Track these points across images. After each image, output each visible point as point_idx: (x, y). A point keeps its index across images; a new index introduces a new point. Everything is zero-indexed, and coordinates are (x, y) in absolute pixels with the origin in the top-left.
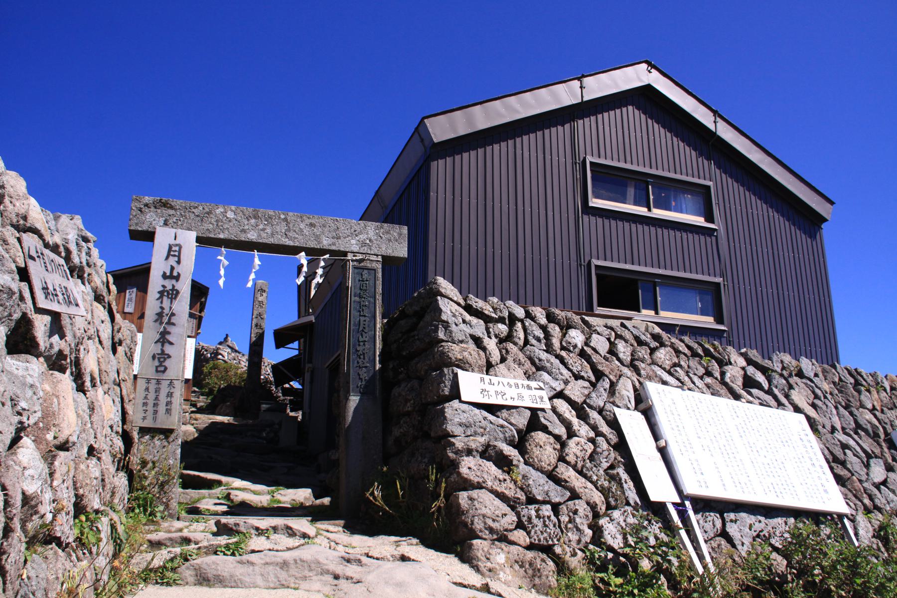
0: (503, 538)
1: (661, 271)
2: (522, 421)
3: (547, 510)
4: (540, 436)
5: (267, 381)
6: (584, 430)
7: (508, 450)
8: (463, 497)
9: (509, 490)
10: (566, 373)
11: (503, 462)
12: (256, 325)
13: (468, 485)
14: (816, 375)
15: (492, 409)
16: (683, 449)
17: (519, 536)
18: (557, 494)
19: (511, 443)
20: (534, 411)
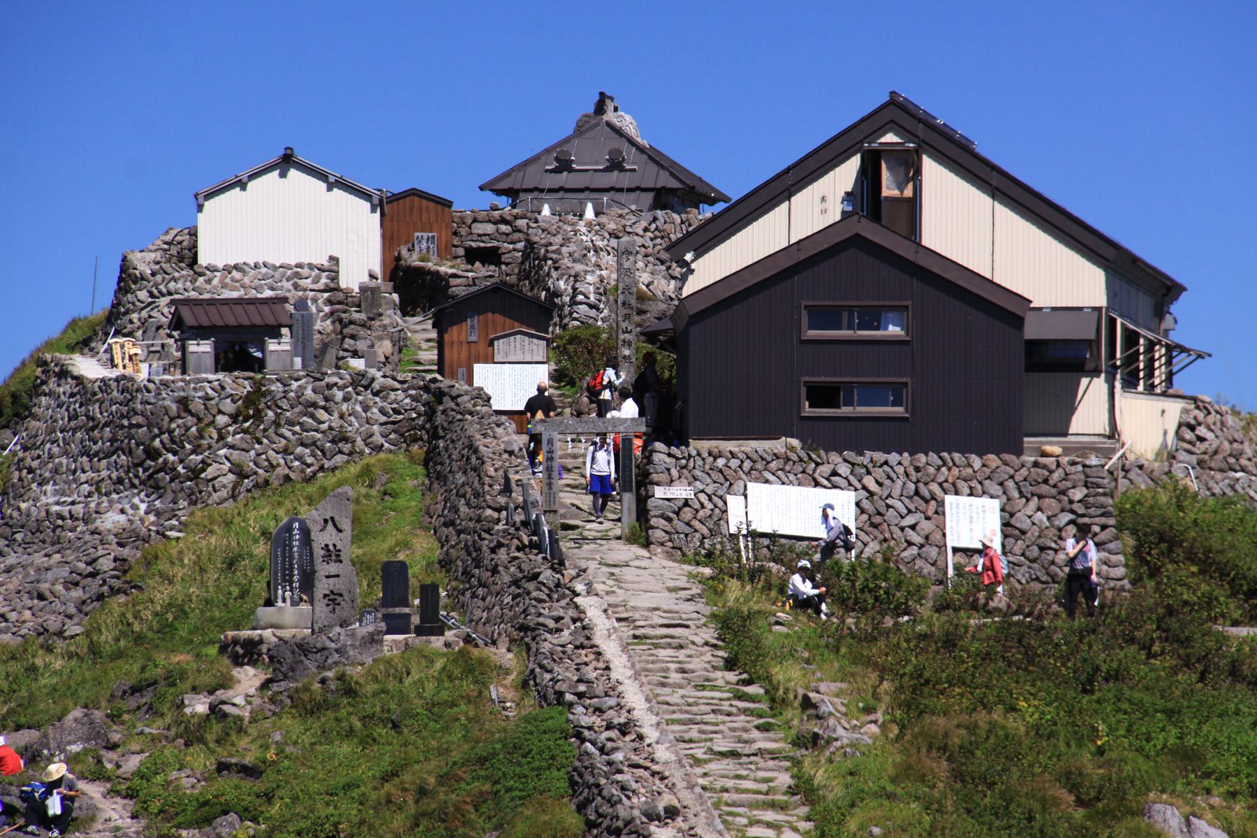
0: (662, 544)
1: (856, 380)
2: (680, 504)
3: (682, 536)
4: (687, 509)
5: (886, 328)
6: (710, 506)
7: (672, 515)
8: (650, 532)
9: (669, 528)
10: (709, 480)
11: (669, 520)
12: (624, 304)
13: (653, 528)
14: (1214, 424)
15: (669, 500)
16: (975, 516)
17: (670, 544)
18: (687, 530)
19: (674, 512)
20: (686, 500)
